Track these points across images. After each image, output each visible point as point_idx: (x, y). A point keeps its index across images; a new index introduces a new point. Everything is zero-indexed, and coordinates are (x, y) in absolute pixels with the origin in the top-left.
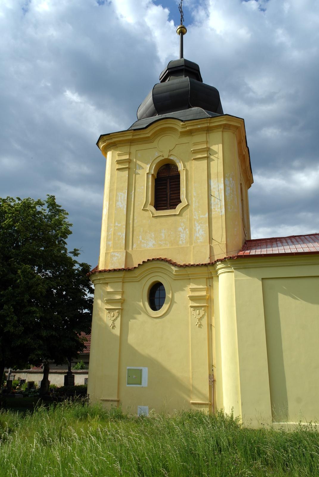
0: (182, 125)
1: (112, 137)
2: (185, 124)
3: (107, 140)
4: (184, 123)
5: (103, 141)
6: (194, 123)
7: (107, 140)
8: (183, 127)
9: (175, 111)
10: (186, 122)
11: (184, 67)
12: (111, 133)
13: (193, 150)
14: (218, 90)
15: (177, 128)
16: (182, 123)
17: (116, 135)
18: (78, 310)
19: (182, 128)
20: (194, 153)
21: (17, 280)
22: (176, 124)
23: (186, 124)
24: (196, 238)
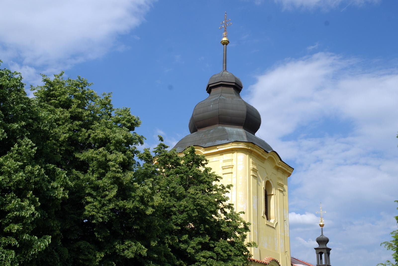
0: (279, 162)
1: (255, 148)
2: (280, 163)
3: (250, 146)
4: (280, 162)
5: (246, 145)
6: (283, 164)
7: (250, 146)
8: (279, 163)
9: (250, 132)
10: (281, 162)
11: (234, 84)
12: (256, 145)
13: (279, 183)
14: (261, 127)
15: (276, 162)
16: (280, 161)
17: (257, 147)
18: (29, 134)
19: (278, 164)
20: (279, 185)
21: (208, 225)
22: (276, 158)
23: (282, 163)
24: (6, 73)
